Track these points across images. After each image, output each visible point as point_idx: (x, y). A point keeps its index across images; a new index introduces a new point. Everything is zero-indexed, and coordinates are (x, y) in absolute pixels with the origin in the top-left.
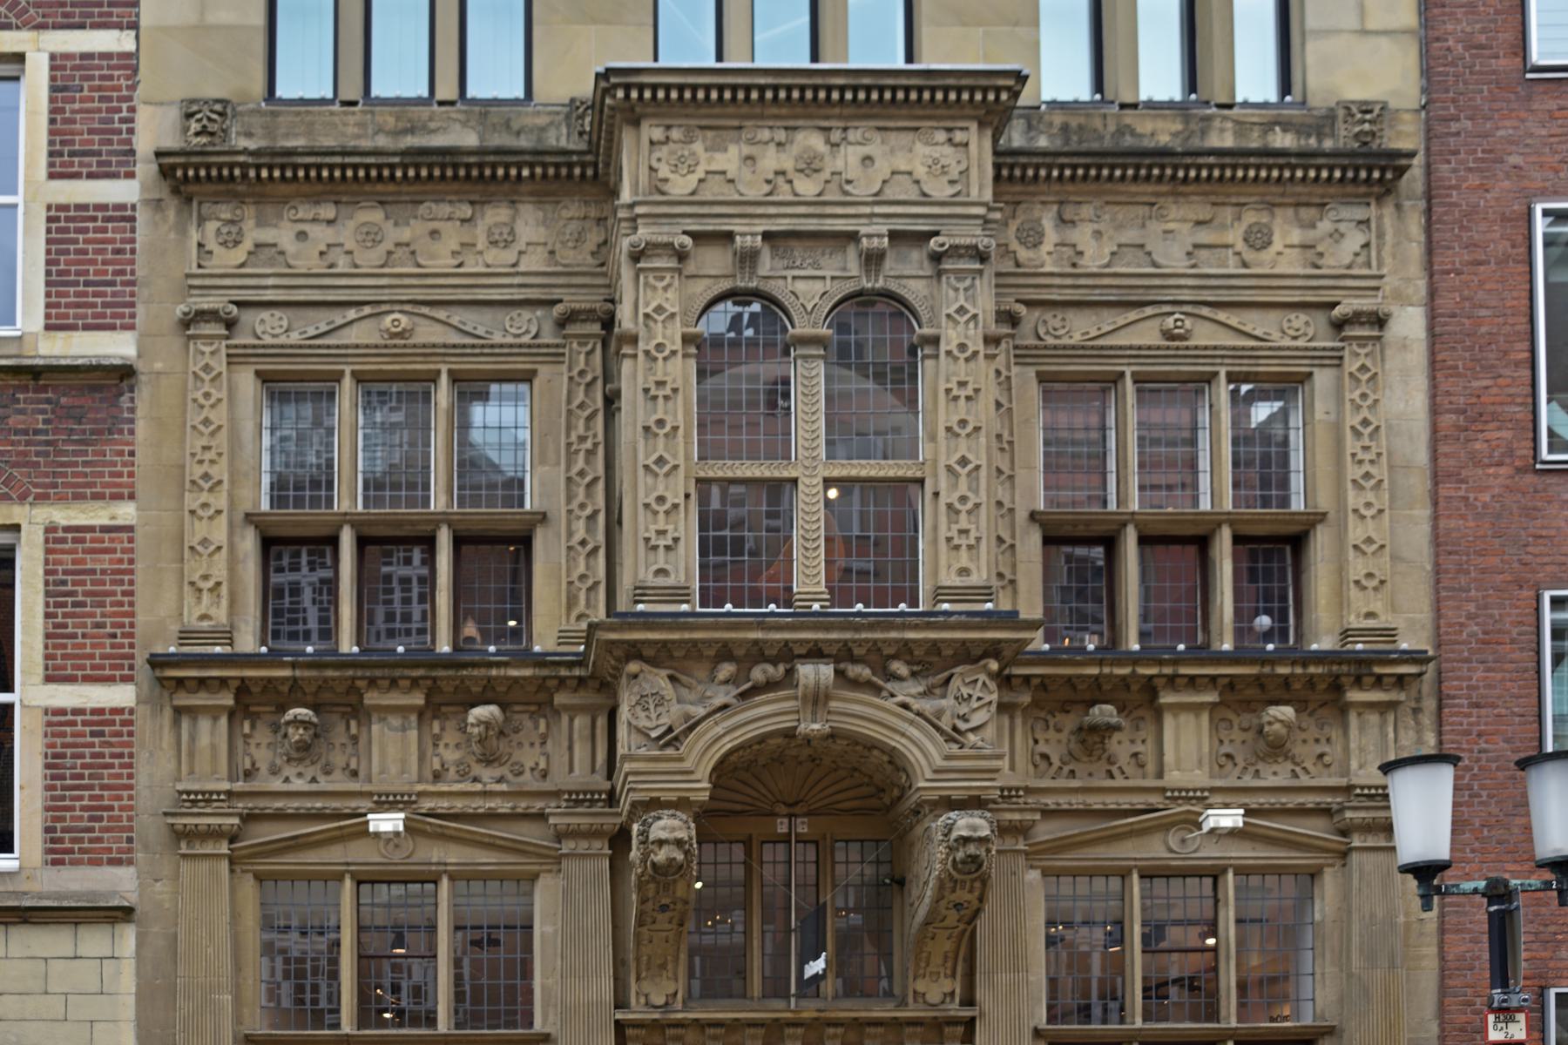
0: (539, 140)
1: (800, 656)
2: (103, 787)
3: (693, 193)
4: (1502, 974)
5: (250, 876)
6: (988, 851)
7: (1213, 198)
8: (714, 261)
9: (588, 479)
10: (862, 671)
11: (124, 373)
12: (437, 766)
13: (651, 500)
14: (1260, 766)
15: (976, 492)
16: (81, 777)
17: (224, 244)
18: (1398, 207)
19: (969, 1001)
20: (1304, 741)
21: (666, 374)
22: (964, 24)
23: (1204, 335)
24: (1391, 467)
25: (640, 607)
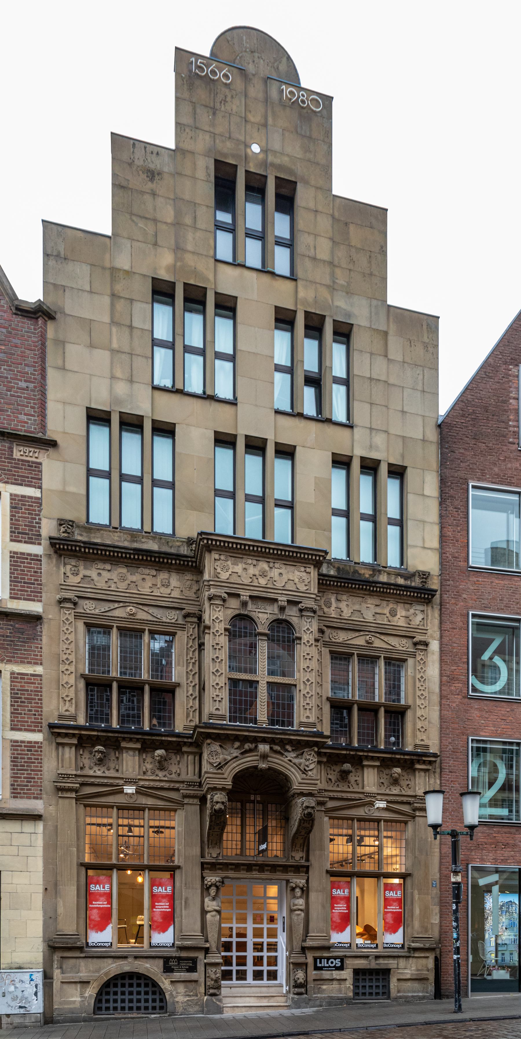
0: (178, 551)
1: (259, 742)
2: (31, 770)
3: (228, 579)
4: (455, 861)
5: (82, 806)
6: (314, 811)
7: (381, 598)
8: (234, 603)
9: (193, 673)
10: (277, 748)
12: (145, 770)
13: (214, 684)
14: (391, 787)
15: (312, 691)
16: (24, 766)
17: (73, 574)
18: (432, 607)
19: (307, 860)
21: (219, 641)
22: (309, 528)
23: (377, 643)
24: (429, 693)
25: (211, 721)
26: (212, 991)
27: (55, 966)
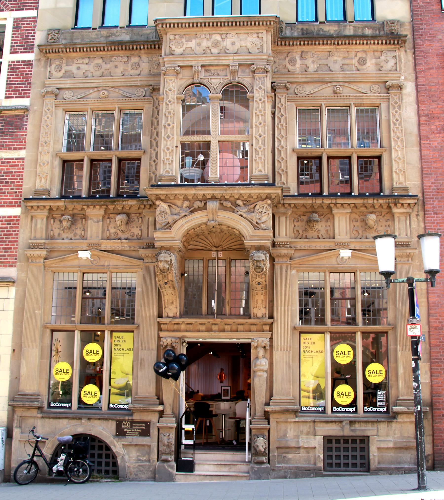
2: (9, 242)
8: (186, 73)
11: (26, 109)
17: (56, 71)
18: (405, 51)
20: (382, 226)
26: (164, 457)
27: (15, 425)
